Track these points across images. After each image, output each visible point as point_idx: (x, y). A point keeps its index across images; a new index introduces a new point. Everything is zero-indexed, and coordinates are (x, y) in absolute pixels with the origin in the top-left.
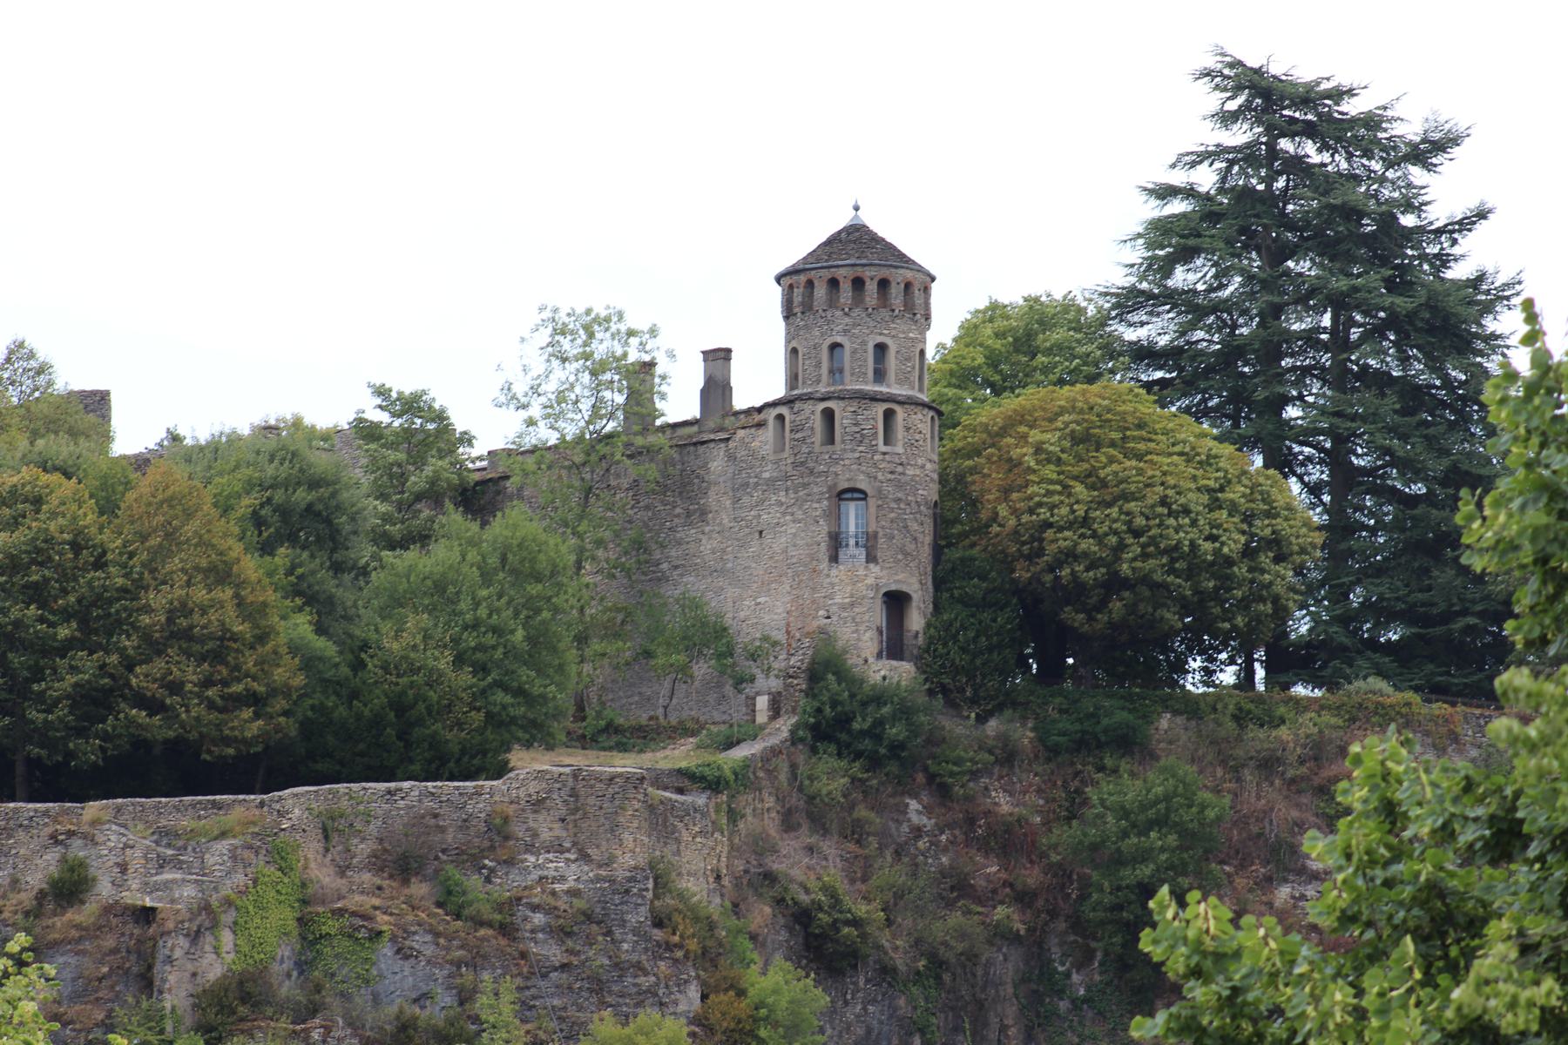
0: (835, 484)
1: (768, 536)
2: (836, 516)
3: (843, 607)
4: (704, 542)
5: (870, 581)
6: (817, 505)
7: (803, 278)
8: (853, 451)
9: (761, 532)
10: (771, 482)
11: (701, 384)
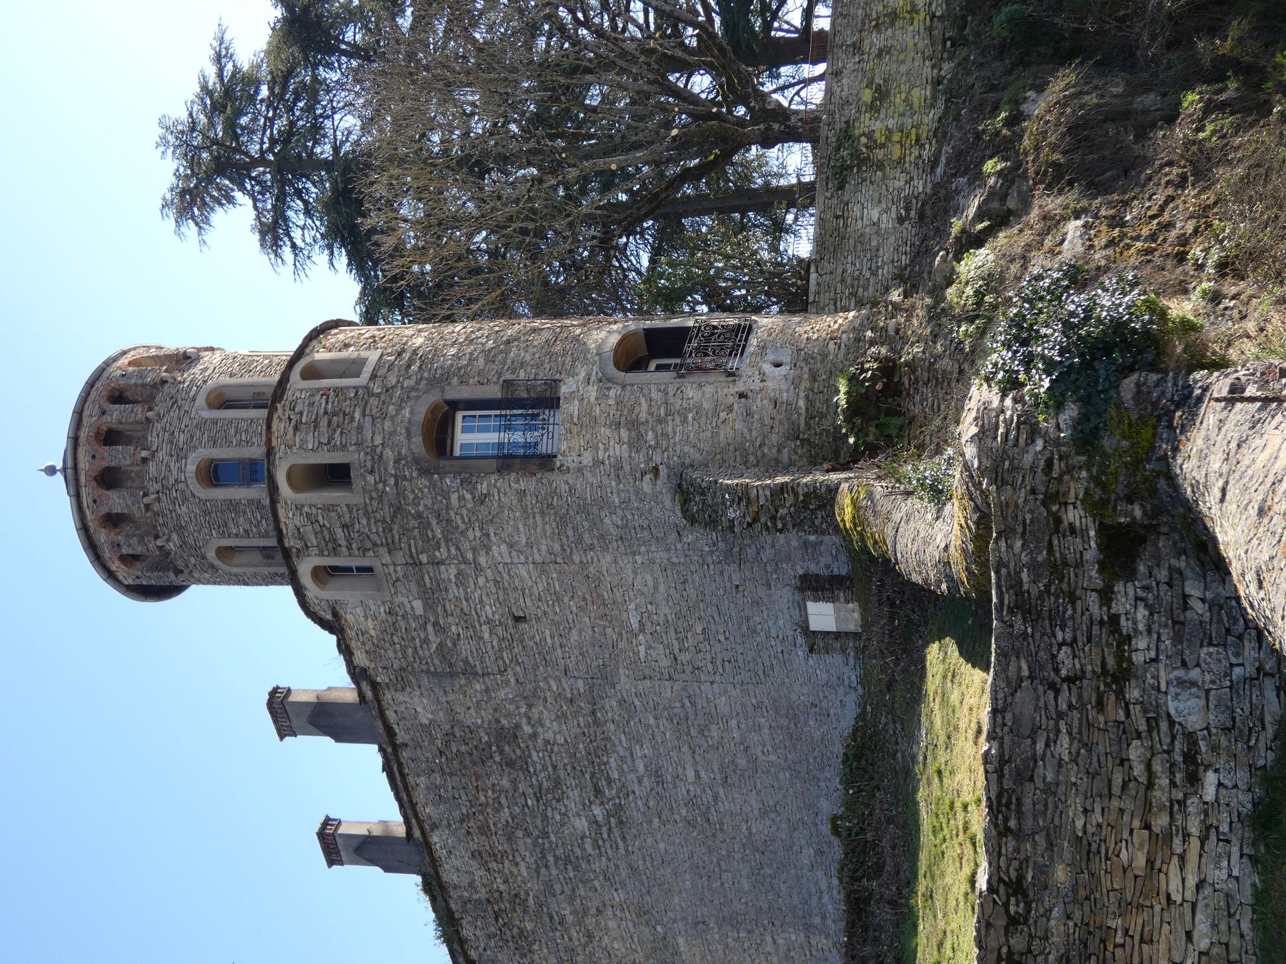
0: (416, 461)
1: (528, 606)
2: (471, 465)
3: (636, 443)
4: (549, 736)
5: (592, 392)
6: (454, 497)
7: (102, 537)
8: (360, 428)
9: (518, 619)
10: (431, 596)
11: (328, 740)
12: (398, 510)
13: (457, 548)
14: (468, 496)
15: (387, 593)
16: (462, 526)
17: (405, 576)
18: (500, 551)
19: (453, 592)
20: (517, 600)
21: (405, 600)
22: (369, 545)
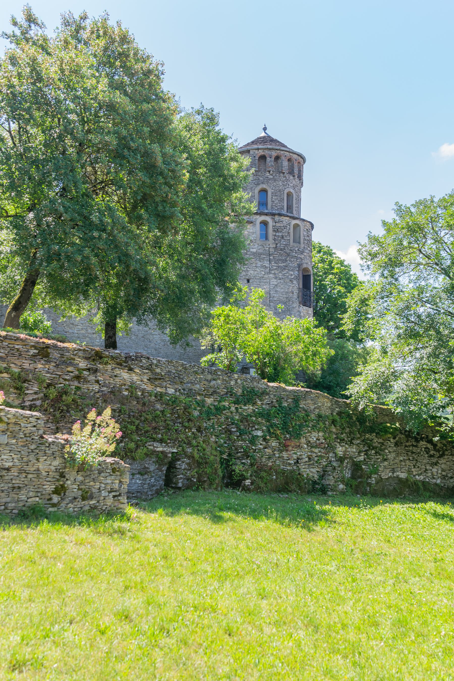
6: (292, 273)
12: (288, 255)
13: (275, 269)
14: (292, 277)
15: (259, 242)
16: (283, 273)
17: (265, 250)
18: (274, 282)
19: (259, 264)
20: (256, 282)
21: (256, 247)
22: (276, 242)
